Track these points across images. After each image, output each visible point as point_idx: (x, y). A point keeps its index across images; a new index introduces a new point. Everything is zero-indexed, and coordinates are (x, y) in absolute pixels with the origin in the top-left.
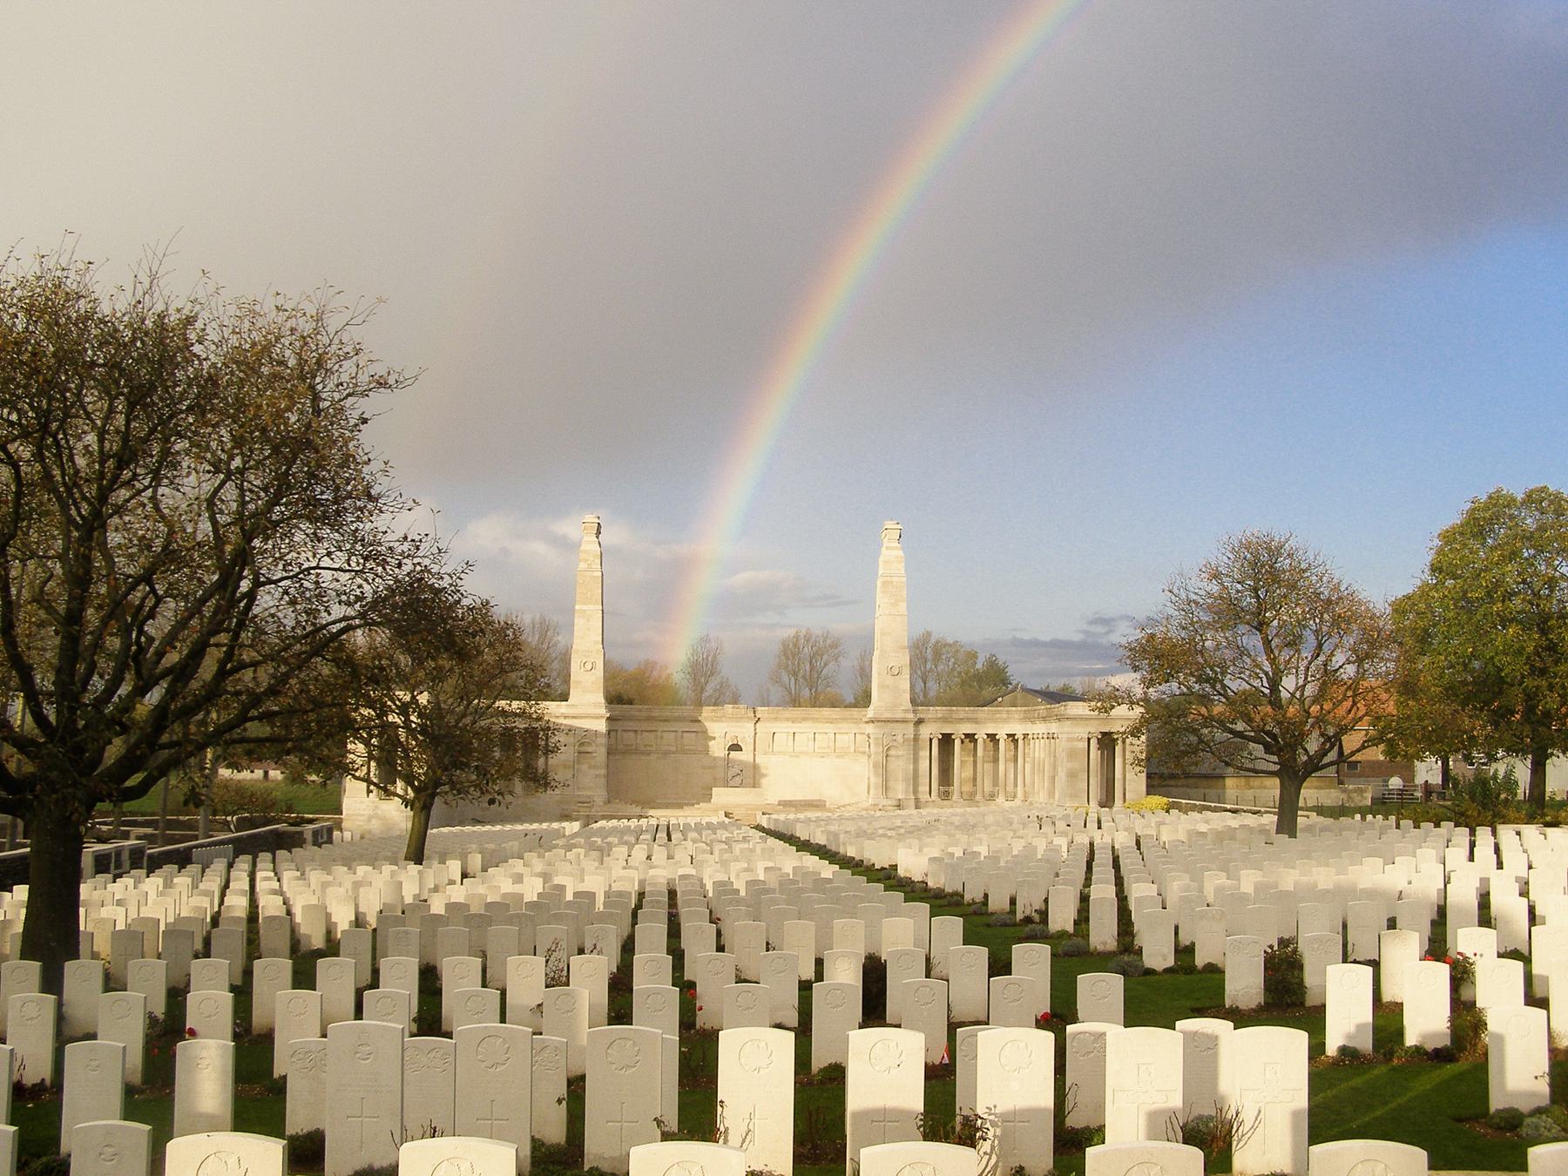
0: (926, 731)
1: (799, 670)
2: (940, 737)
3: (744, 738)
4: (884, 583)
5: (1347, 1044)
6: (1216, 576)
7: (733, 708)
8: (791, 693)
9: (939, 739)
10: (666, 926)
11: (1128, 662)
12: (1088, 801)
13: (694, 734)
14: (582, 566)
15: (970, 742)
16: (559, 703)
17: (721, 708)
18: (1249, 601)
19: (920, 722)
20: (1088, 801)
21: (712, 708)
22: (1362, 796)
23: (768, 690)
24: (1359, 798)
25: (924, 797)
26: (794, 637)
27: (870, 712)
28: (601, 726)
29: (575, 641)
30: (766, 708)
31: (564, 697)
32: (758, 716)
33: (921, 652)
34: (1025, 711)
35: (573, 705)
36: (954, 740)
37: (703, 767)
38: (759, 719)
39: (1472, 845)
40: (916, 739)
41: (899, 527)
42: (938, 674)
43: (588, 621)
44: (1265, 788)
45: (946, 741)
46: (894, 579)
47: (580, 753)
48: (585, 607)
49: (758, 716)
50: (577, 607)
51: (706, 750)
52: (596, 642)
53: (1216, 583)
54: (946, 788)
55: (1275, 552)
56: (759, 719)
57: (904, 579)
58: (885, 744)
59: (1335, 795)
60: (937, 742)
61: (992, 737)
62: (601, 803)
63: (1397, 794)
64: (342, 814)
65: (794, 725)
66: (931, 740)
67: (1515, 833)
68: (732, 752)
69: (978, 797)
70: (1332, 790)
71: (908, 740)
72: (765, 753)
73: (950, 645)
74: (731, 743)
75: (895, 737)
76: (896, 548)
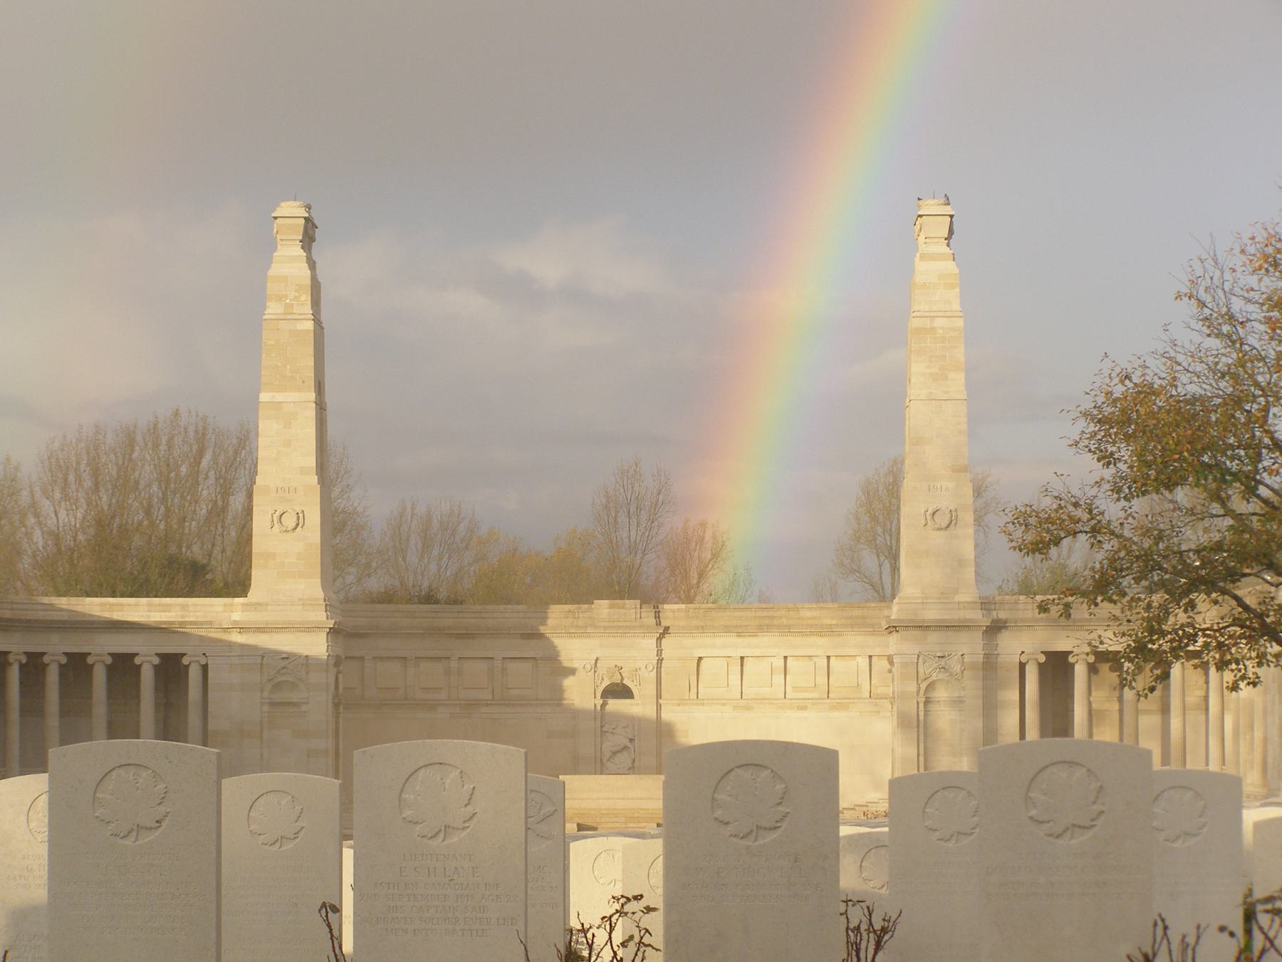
7: (611, 607)
9: (1040, 665)
10: (313, 375)
13: (529, 665)
14: (273, 309)
15: (1112, 669)
27: (895, 611)
28: (317, 646)
30: (683, 606)
31: (237, 585)
32: (665, 623)
35: (258, 604)
36: (187, 667)
38: (667, 629)
39: (511, 688)
40: (989, 665)
41: (948, 210)
46: (939, 323)
47: (274, 704)
48: (280, 397)
49: (665, 623)
50: (264, 397)
51: (556, 697)
57: (960, 323)
58: (922, 676)
65: (740, 640)
72: (682, 702)
74: (606, 683)
75: (943, 662)
76: (940, 257)
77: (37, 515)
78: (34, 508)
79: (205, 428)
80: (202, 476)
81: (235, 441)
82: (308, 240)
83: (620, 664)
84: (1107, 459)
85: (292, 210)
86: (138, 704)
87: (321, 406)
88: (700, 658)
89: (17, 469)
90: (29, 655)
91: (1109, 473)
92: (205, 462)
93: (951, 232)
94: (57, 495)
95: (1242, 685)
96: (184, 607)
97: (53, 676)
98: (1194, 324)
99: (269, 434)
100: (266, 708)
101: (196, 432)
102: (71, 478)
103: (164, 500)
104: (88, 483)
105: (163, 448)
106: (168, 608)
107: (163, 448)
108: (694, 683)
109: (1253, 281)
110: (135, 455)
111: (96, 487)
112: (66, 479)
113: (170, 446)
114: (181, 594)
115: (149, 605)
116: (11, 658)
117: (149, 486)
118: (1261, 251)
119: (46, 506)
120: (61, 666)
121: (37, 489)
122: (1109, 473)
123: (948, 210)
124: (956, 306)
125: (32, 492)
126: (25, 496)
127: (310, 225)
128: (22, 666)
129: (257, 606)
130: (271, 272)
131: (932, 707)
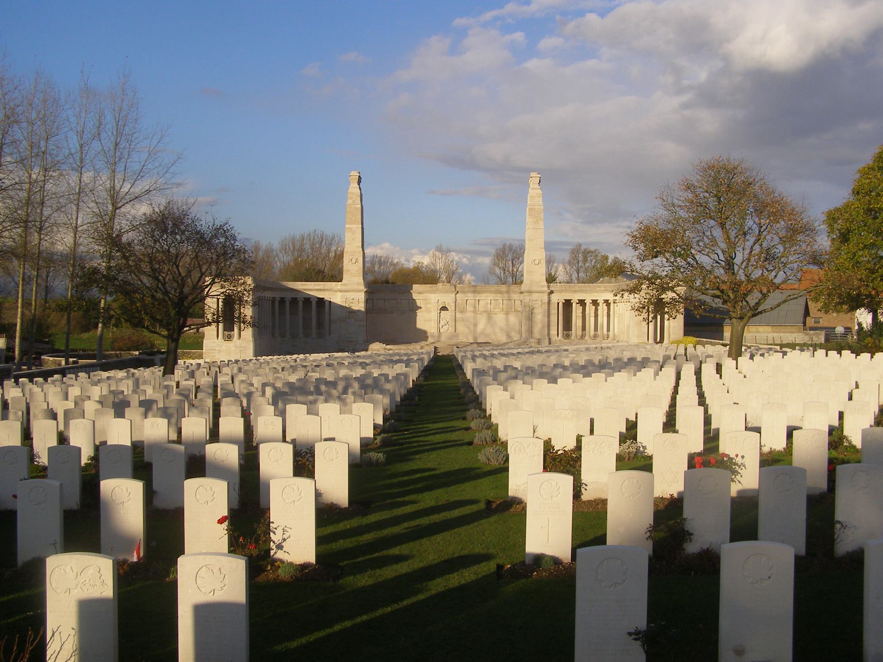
0: (555, 298)
1: (506, 267)
2: (564, 301)
3: (449, 303)
4: (529, 209)
5: (808, 472)
6: (689, 187)
8: (501, 280)
9: (563, 303)
11: (631, 244)
12: (648, 340)
14: (349, 201)
16: (337, 283)
17: (435, 285)
18: (712, 203)
19: (552, 292)
20: (648, 340)
21: (430, 285)
22: (818, 337)
23: (488, 278)
24: (817, 339)
25: (554, 338)
26: (502, 248)
29: (346, 246)
33: (576, 256)
34: (615, 286)
35: (345, 284)
37: (425, 321)
38: (458, 292)
41: (539, 176)
42: (586, 269)
43: (353, 234)
44: (758, 332)
45: (568, 304)
46: (536, 207)
48: (351, 226)
52: (358, 247)
53: (689, 191)
54: (568, 332)
55: (732, 171)
56: (458, 292)
57: (542, 207)
59: (801, 337)
60: (562, 305)
61: (582, 303)
62: (362, 342)
63: (840, 337)
64: (202, 350)
66: (558, 303)
67: (872, 359)
68: (442, 311)
69: (587, 338)
70: (800, 334)
71: (545, 303)
73: (592, 252)
77: (278, 257)
78: (277, 255)
79: (323, 235)
80: (322, 247)
81: (331, 238)
82: (359, 182)
83: (445, 301)
84: (636, 248)
85: (355, 174)
86: (311, 312)
87: (363, 229)
88: (467, 300)
89: (273, 245)
90: (281, 298)
91: (637, 253)
92: (323, 244)
93: (540, 182)
94: (284, 252)
95: (671, 319)
96: (324, 285)
97: (288, 303)
98: (660, 207)
99: (348, 236)
100: (347, 313)
101: (321, 235)
102: (287, 247)
103: (312, 254)
104: (292, 249)
105: (312, 239)
106: (320, 285)
107: (312, 239)
108: (465, 307)
109: (681, 194)
110: (304, 242)
111: (294, 251)
112: (286, 248)
113: (314, 239)
114: (320, 278)
115: (314, 284)
116: (276, 299)
117: (308, 250)
118: (17, 234)
119: (281, 255)
120: (290, 301)
121: (278, 251)
122: (637, 253)
123: (539, 176)
124: (541, 202)
125: (277, 252)
126: (275, 253)
127: (360, 178)
128: (279, 301)
129: (345, 285)
130: (349, 191)
131: (533, 314)
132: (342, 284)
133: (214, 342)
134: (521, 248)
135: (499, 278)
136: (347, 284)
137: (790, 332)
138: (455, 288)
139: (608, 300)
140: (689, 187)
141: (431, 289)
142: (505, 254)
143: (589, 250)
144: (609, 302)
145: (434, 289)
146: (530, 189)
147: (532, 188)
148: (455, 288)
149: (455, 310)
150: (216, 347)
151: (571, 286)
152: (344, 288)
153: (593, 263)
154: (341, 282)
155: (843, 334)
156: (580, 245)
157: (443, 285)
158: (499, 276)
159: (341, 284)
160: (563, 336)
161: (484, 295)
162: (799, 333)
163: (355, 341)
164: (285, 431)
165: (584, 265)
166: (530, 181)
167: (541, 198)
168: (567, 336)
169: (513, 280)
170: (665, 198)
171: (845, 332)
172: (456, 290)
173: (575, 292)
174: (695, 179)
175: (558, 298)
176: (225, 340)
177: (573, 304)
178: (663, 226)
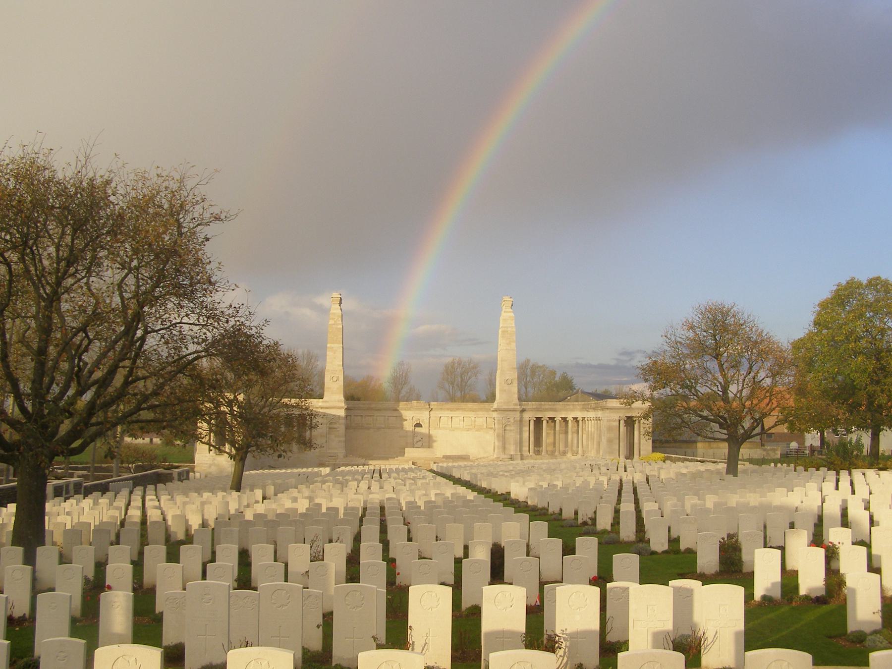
0: (527, 416)
1: (455, 381)
2: (535, 419)
6: (692, 327)
11: (642, 376)
14: (331, 322)
24: (773, 454)
35: (326, 401)
38: (432, 409)
45: (538, 421)
46: (509, 329)
48: (333, 345)
52: (339, 366)
55: (725, 314)
56: (432, 409)
57: (514, 330)
62: (342, 457)
63: (795, 452)
64: (194, 463)
66: (530, 421)
68: (416, 428)
93: (512, 305)
129: (326, 402)
132: (324, 401)
133: (206, 456)
134: (470, 362)
135: (447, 391)
136: (328, 401)
137: (749, 448)
138: (429, 405)
139: (577, 418)
140: (692, 327)
141: (406, 406)
142: (454, 369)
143: (537, 365)
144: (578, 420)
145: (409, 407)
146: (503, 312)
147: (505, 312)
148: (429, 405)
149: (429, 427)
150: (207, 461)
151: (542, 404)
152: (325, 405)
153: (541, 377)
154: (322, 399)
155: (797, 449)
156: (528, 361)
157: (417, 403)
158: (448, 390)
159: (322, 401)
160: (534, 453)
161: (458, 412)
162: (756, 448)
163: (335, 456)
164: (143, 553)
165: (532, 379)
166: (502, 304)
167: (514, 321)
168: (538, 453)
169: (461, 395)
170: (669, 336)
171: (799, 447)
172: (430, 407)
173: (546, 410)
174: (696, 318)
175: (529, 416)
176: (216, 455)
177: (544, 422)
178: (669, 361)
